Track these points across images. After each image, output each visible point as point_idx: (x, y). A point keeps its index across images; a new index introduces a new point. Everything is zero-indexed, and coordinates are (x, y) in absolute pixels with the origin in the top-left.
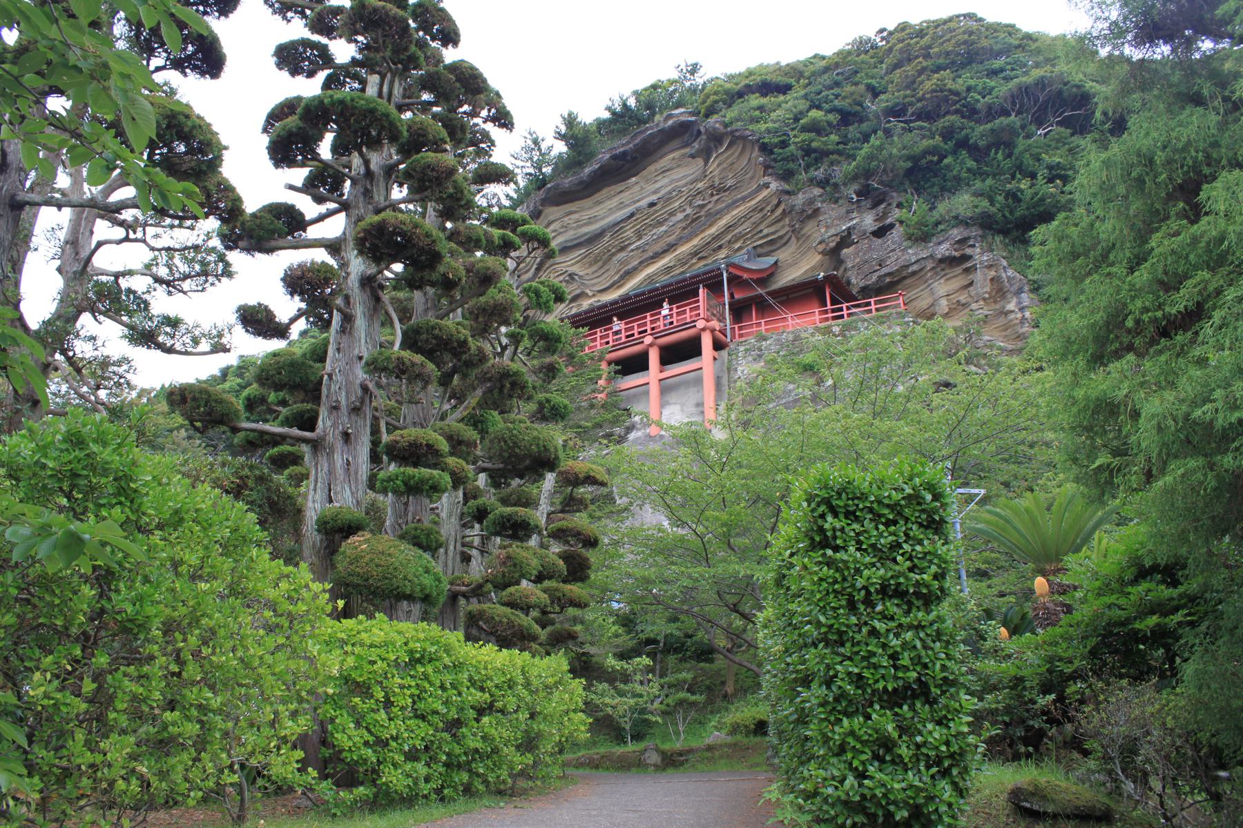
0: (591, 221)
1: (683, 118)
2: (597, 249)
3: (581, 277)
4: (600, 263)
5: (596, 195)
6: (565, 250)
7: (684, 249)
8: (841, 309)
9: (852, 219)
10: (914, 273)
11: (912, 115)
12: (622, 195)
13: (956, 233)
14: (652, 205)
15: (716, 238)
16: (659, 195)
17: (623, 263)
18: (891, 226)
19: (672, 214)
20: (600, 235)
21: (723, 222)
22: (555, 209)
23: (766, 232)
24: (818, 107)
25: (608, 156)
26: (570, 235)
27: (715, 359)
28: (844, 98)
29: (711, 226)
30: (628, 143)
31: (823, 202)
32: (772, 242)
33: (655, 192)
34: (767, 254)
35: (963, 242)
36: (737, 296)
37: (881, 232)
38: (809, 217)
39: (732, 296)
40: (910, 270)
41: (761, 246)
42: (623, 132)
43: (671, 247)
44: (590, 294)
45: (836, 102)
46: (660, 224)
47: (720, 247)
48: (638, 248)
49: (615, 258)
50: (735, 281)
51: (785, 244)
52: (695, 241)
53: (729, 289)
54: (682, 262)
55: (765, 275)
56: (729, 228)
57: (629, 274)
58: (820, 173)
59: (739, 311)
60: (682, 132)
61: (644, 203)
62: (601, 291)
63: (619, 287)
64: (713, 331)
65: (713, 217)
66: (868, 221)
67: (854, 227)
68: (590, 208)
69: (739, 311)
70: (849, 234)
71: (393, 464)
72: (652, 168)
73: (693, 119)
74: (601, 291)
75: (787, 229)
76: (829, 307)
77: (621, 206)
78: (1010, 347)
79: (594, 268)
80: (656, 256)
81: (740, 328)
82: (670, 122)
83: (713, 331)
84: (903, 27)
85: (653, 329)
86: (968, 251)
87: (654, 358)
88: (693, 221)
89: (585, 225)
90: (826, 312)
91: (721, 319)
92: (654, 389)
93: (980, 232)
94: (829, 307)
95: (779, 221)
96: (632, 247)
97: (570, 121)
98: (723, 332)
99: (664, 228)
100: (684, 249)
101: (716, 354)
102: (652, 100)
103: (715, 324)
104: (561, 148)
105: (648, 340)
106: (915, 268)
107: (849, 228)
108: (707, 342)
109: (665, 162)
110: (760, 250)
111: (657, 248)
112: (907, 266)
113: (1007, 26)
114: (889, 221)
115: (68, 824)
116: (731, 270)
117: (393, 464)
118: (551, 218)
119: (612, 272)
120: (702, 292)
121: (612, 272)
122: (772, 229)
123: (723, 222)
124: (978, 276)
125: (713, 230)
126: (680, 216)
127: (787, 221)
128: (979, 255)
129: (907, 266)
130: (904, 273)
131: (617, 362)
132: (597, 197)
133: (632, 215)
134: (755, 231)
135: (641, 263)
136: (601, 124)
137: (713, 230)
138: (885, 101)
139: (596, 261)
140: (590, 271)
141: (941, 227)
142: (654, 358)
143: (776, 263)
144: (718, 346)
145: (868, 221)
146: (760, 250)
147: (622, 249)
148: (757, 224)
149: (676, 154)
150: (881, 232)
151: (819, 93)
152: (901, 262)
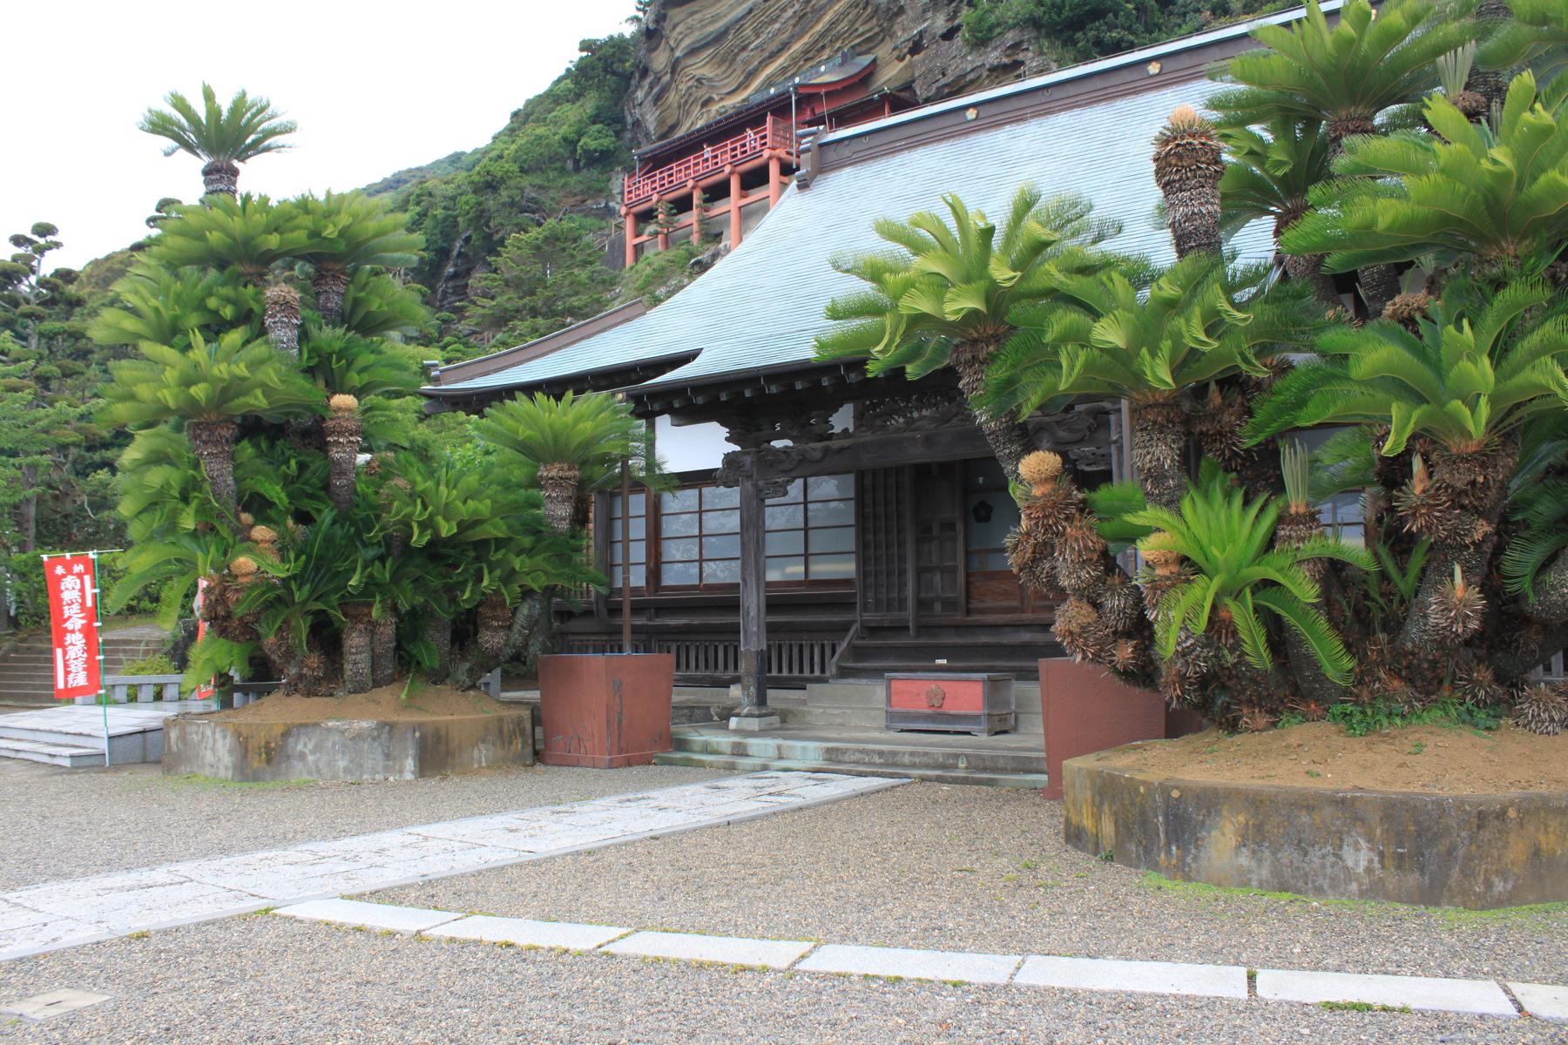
0: (714, 19)
3: (709, 80)
6: (693, 51)
7: (797, 47)
10: (972, 82)
13: (1011, 37)
15: (823, 35)
17: (747, 63)
18: (958, 28)
19: (783, 10)
21: (827, 18)
23: (861, 30)
26: (696, 36)
29: (818, 21)
32: (869, 40)
34: (867, 52)
35: (1016, 46)
37: (949, 35)
40: (968, 78)
43: (785, 46)
46: (774, 21)
47: (823, 47)
49: (739, 58)
52: (806, 39)
56: (833, 24)
57: (751, 75)
62: (729, 93)
63: (746, 88)
64: (779, 159)
67: (925, 30)
74: (729, 93)
75: (877, 29)
79: (723, 68)
80: (773, 56)
86: (1021, 57)
87: (697, 198)
88: (801, 18)
92: (734, 216)
93: (1034, 34)
99: (777, 26)
100: (797, 47)
105: (766, 153)
106: (972, 76)
108: (774, 169)
110: (858, 49)
111: (773, 47)
112: (965, 75)
114: (957, 22)
115: (5, 339)
118: (676, 20)
119: (738, 72)
120: (769, 119)
121: (738, 72)
123: (827, 18)
125: (819, 27)
126: (790, 12)
127: (874, 21)
129: (965, 75)
130: (962, 83)
133: (750, 11)
134: (852, 30)
137: (819, 27)
139: (723, 61)
140: (719, 71)
141: (998, 30)
143: (874, 60)
146: (858, 49)
147: (744, 48)
148: (853, 23)
150: (949, 35)
152: (958, 72)
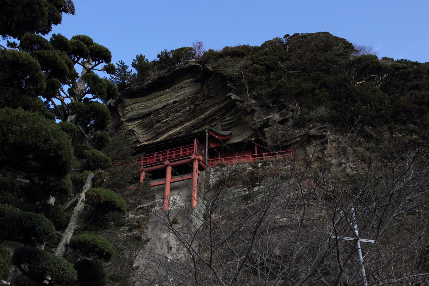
1: (193, 64)
2: (146, 121)
4: (147, 128)
5: (149, 96)
8: (262, 156)
9: (269, 115)
11: (300, 70)
12: (161, 97)
14: (175, 102)
16: (179, 99)
20: (149, 114)
22: (129, 100)
23: (227, 119)
24: (257, 63)
25: (156, 77)
27: (199, 175)
28: (269, 60)
29: (201, 114)
30: (166, 73)
31: (256, 106)
33: (178, 96)
36: (212, 146)
37: (283, 122)
38: (249, 113)
39: (209, 146)
41: (225, 125)
42: (163, 68)
43: (182, 123)
44: (141, 141)
45: (265, 62)
48: (166, 122)
50: (211, 138)
51: (236, 125)
52: (193, 121)
53: (208, 142)
54: (186, 129)
55: (225, 138)
58: (255, 93)
59: (212, 154)
60: (192, 71)
61: (171, 102)
64: (199, 160)
65: (203, 111)
66: (277, 117)
68: (145, 101)
69: (212, 154)
70: (268, 122)
71: (308, 148)
72: (176, 86)
73: (198, 65)
76: (256, 154)
77: (160, 102)
78: (41, 216)
80: (176, 126)
81: (212, 161)
82: (187, 65)
83: (199, 160)
84: (296, 35)
85: (169, 157)
87: (169, 171)
89: (142, 109)
90: (255, 156)
91: (203, 156)
94: (256, 154)
95: (234, 114)
96: (164, 121)
97: (141, 58)
98: (204, 162)
101: (200, 172)
102: (182, 54)
103: (201, 158)
104: (135, 71)
107: (268, 119)
108: (196, 165)
109: (182, 84)
113: (343, 39)
116: (210, 133)
117: (308, 148)
120: (195, 142)
122: (230, 118)
124: (329, 146)
128: (330, 135)
131: (150, 172)
132: (149, 96)
133: (165, 106)
135: (167, 129)
136: (154, 62)
138: (288, 63)
142: (169, 171)
144: (201, 168)
145: (277, 117)
149: (188, 81)
151: (257, 58)
